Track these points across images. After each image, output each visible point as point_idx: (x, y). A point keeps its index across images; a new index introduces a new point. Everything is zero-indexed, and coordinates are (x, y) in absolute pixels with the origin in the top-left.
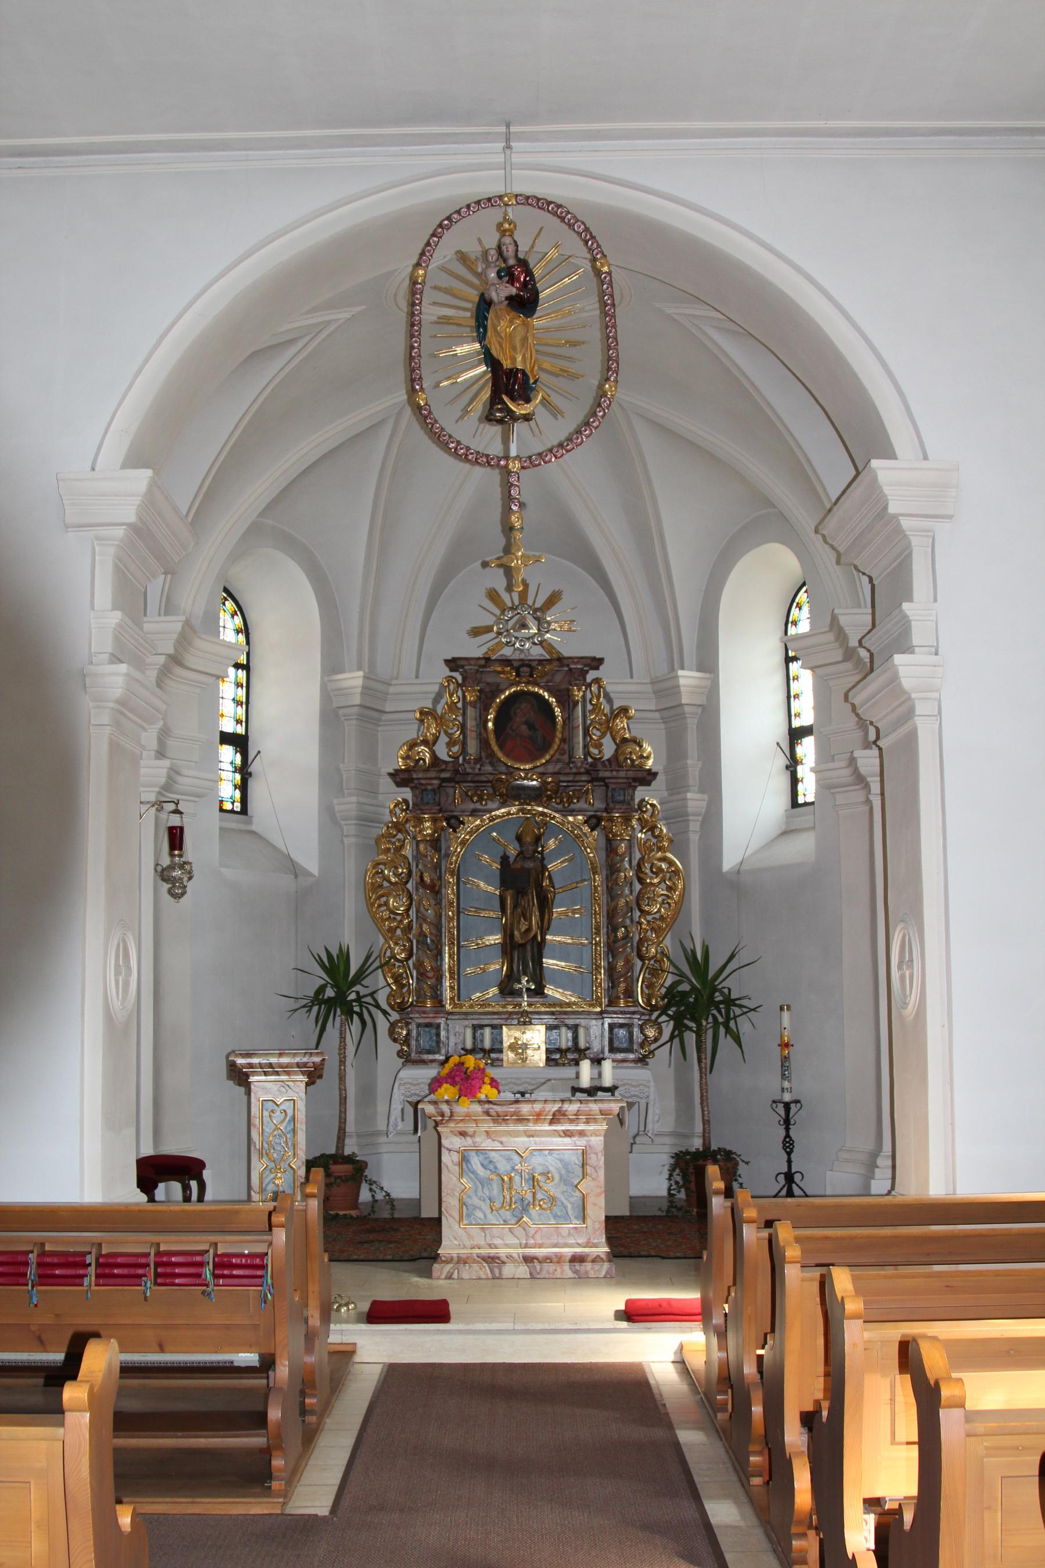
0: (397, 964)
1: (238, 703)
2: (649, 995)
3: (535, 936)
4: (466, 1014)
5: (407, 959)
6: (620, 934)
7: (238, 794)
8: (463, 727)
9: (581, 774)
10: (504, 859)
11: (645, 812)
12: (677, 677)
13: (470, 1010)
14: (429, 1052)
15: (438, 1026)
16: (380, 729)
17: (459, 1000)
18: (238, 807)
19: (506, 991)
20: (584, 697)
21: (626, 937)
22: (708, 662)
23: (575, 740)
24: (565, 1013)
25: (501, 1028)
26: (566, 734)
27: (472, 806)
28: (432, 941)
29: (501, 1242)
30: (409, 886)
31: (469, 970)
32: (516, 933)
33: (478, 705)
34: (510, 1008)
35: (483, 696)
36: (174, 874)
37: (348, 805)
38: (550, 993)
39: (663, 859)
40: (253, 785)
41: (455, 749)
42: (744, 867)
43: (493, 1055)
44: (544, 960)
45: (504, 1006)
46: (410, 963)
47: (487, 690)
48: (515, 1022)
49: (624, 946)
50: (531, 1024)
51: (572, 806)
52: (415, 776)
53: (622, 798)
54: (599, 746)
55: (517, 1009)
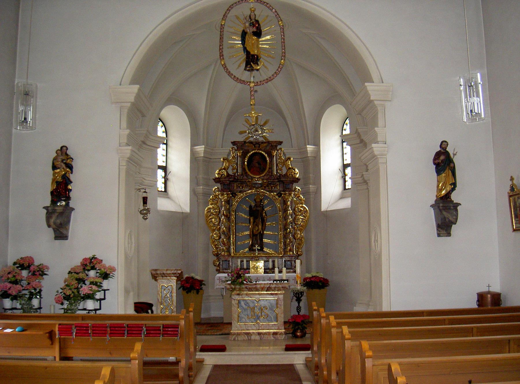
3: (260, 232)
10: (250, 207)
14: (226, 269)
15: (229, 261)
18: (163, 190)
22: (317, 143)
24: (270, 257)
30: (219, 215)
34: (252, 255)
40: (169, 184)
54: (281, 170)
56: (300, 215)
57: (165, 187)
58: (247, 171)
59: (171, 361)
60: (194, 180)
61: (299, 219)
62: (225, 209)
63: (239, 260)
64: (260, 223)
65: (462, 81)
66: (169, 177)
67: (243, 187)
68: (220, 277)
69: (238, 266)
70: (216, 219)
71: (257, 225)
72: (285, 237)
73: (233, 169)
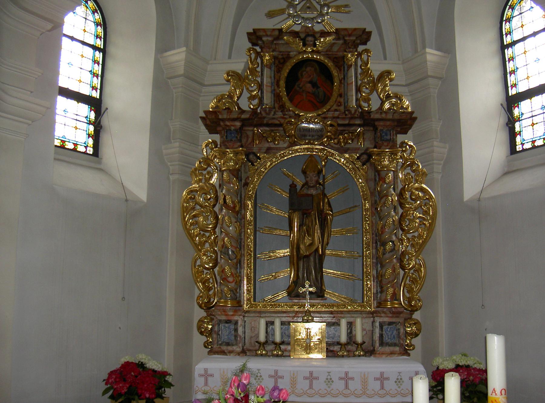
0: (205, 271)
1: (95, 75)
2: (409, 298)
3: (317, 250)
4: (260, 312)
6: (388, 247)
7: (91, 142)
8: (260, 87)
9: (356, 118)
10: (293, 186)
12: (425, 53)
13: (263, 309)
14: (228, 344)
15: (236, 323)
16: (201, 98)
17: (255, 300)
18: (90, 151)
19: (293, 294)
20: (356, 62)
21: (393, 250)
22: (446, 44)
23: (349, 94)
24: (342, 312)
26: (342, 91)
27: (267, 145)
28: (233, 252)
29: (264, 34)
30: (217, 209)
31: (263, 277)
32: (302, 246)
33: (273, 68)
34: (296, 308)
35: (277, 62)
37: (174, 148)
38: (328, 296)
39: (422, 190)
40: (105, 138)
41: (256, 102)
42: (485, 195)
43: (283, 347)
45: (291, 307)
46: (216, 270)
47: (280, 57)
49: (391, 258)
51: (347, 146)
52: (220, 117)
53: (388, 137)
54: (367, 100)
55: (302, 309)
56: (416, 209)
57: (96, 146)
58: (285, 99)
60: (159, 131)
61: (412, 221)
62: (228, 190)
63: (263, 322)
64: (317, 227)
65: (421, 167)
66: (105, 121)
67: (274, 140)
68: (206, 370)
69: (258, 336)
70: (206, 218)
72: (379, 262)
73: (252, 98)
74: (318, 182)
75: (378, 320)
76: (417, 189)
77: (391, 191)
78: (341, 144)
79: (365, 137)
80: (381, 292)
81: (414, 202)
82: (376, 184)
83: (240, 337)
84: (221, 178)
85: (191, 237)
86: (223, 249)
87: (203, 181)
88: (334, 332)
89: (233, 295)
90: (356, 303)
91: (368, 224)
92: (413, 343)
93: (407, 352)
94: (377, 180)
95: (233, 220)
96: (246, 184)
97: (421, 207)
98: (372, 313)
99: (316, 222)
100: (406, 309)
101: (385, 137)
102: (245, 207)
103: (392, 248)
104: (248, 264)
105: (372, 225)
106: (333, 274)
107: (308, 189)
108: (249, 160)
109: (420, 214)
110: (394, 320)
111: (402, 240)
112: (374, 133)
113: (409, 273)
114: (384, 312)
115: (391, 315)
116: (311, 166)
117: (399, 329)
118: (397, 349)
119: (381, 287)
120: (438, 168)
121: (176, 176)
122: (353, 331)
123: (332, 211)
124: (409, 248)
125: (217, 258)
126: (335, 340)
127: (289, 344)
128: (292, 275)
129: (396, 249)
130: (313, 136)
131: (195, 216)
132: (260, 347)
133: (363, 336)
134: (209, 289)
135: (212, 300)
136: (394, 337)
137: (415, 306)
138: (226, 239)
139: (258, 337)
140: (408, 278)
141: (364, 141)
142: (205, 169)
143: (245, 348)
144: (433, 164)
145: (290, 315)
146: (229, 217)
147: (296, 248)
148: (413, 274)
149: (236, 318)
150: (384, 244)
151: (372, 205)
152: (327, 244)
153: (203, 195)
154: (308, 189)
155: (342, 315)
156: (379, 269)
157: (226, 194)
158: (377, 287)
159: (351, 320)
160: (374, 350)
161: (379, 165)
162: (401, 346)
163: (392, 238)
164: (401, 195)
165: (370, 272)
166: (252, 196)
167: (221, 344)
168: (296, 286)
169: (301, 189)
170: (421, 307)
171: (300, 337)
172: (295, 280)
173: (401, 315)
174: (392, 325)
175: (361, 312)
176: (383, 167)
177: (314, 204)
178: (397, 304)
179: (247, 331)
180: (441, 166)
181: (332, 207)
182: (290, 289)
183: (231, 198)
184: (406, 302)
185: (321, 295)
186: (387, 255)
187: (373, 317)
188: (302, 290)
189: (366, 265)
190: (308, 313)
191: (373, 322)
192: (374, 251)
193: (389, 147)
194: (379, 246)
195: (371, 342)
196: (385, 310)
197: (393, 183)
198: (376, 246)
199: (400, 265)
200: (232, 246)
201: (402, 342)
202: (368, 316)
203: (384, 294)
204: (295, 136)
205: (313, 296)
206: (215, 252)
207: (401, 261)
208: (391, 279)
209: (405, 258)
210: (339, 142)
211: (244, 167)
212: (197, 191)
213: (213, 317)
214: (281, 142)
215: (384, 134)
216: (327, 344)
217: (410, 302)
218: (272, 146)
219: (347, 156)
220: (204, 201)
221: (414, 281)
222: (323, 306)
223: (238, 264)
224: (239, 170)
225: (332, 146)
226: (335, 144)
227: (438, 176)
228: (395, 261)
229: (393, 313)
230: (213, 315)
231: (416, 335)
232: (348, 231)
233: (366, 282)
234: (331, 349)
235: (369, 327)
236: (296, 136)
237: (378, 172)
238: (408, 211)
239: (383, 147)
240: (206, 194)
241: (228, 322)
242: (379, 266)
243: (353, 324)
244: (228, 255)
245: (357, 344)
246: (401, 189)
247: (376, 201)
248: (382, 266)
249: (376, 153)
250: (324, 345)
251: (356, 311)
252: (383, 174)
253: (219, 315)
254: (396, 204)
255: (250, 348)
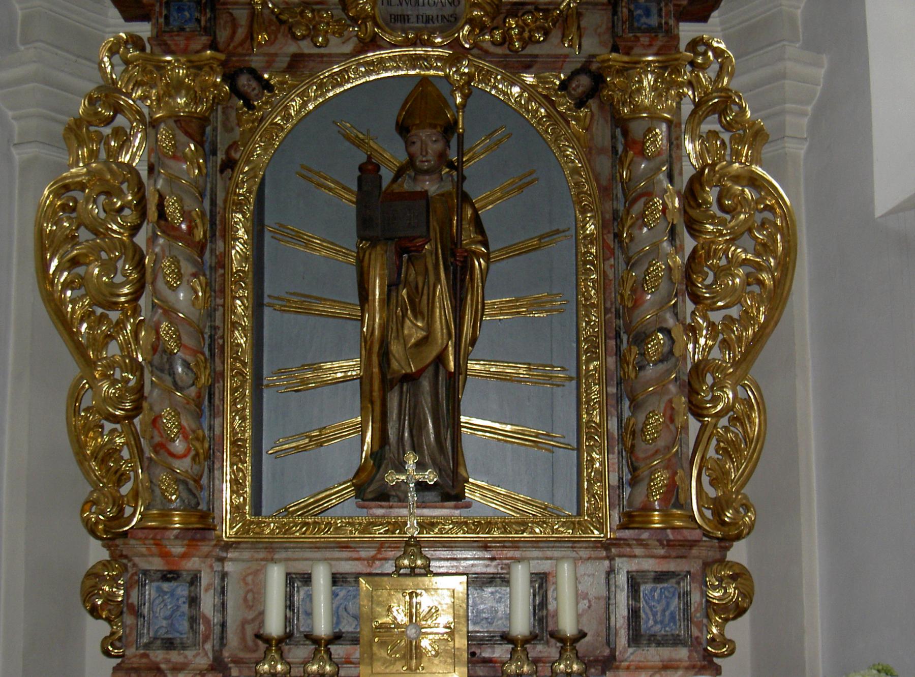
0: (109, 426)
2: (716, 501)
3: (441, 359)
5: (131, 416)
10: (369, 170)
11: (703, 67)
14: (169, 644)
15: (194, 580)
21: (667, 356)
24: (515, 545)
25: (357, 582)
30: (141, 239)
32: (395, 348)
34: (379, 533)
36: (85, 325)
38: (477, 497)
39: (754, 182)
43: (337, 650)
44: (463, 419)
45: (367, 528)
48: (614, 323)
49: (661, 381)
50: (427, 572)
53: (654, 21)
59: (243, 36)
61: (722, 273)
63: (275, 577)
64: (442, 290)
65: (749, 114)
67: (312, 34)
69: (261, 616)
70: (109, 267)
71: (419, 306)
74: (442, 157)
75: (624, 566)
76: (736, 179)
77: (660, 182)
78: (511, 43)
79: (583, 24)
80: (633, 483)
81: (728, 217)
82: (619, 160)
83: (207, 621)
84: (154, 149)
85: (65, 324)
86: (157, 357)
87: (103, 155)
88: (490, 603)
89: (185, 495)
90: (558, 516)
91: (593, 281)
92: (728, 636)
93: (711, 662)
94: (620, 149)
95: (187, 268)
96: (229, 164)
97: (750, 230)
98: (606, 545)
99: (438, 279)
100: (706, 534)
101: (644, 20)
102: (228, 234)
103: (666, 349)
104: (234, 403)
105: (603, 286)
106: (493, 430)
107: (415, 179)
108: (236, 92)
109: (745, 251)
110: (671, 566)
111: (693, 330)
112: (610, 14)
113: (715, 426)
114: (641, 543)
115: (662, 552)
116: (422, 109)
117: (687, 594)
118: (683, 653)
119: (634, 469)
120: (798, 123)
121: (31, 151)
122: (550, 599)
123: (486, 245)
124: (716, 350)
125: (142, 386)
126: (499, 626)
127: (355, 641)
128: (368, 439)
129: (677, 353)
130: (428, 19)
131: (75, 262)
132: (268, 649)
133: (579, 617)
134: (120, 478)
135: (128, 511)
136: (673, 617)
137: (734, 523)
138: (164, 325)
139: (262, 623)
140: (714, 442)
141: (580, 37)
142: (109, 121)
143: (226, 654)
144: (783, 76)
145: (363, 554)
146: (176, 261)
147: (378, 353)
148: (727, 429)
149: (193, 564)
150: (641, 339)
151: (603, 226)
152: (473, 341)
153: (103, 197)
154: (415, 179)
155: (517, 554)
156: (627, 413)
157: (163, 191)
158: (620, 468)
159: (545, 566)
160: (612, 657)
161: (624, 104)
162: (694, 643)
163: (665, 320)
164: (692, 194)
165: (599, 425)
166: (247, 198)
167: (147, 646)
168: (379, 467)
169: (395, 180)
170: (751, 527)
171: (388, 620)
172: (376, 448)
173: (695, 551)
174: (666, 580)
175: (573, 544)
176: (638, 109)
177: (434, 224)
178: (679, 517)
179: (230, 605)
180: (805, 121)
181: (488, 233)
182: (363, 476)
183: (180, 200)
184: (708, 514)
185: (453, 493)
186: (651, 371)
187: (611, 559)
188: (393, 478)
189: (588, 403)
190: (413, 546)
191: (610, 572)
192: (611, 361)
193: (654, 49)
194: (625, 345)
195: (604, 633)
196: (645, 535)
197: (665, 157)
198: (618, 347)
199: (690, 402)
200: (180, 345)
201: (695, 632)
202: (594, 554)
203: (642, 489)
204: (373, 18)
205: (431, 496)
206: (136, 368)
207: (691, 390)
208: (661, 443)
209: (704, 382)
210: (506, 39)
211: (224, 112)
212: (82, 187)
213: (125, 561)
214: (334, 40)
215: (639, 12)
216: (469, 638)
217: (718, 513)
218: (306, 51)
219: (530, 79)
220: (103, 215)
221: (729, 450)
222: (459, 524)
223: (206, 402)
224: (204, 120)
225: (486, 52)
226: (494, 43)
227: (797, 149)
228: (673, 388)
229: (670, 544)
230: (126, 557)
231: (740, 611)
232: (536, 305)
233: (589, 455)
234: (486, 654)
235: (595, 586)
236: (380, 21)
237: (621, 124)
238: (713, 242)
239: (637, 50)
240: (108, 194)
241: (170, 576)
242: (627, 403)
243: (551, 579)
244: (172, 373)
245: (562, 640)
246: (692, 180)
247: (615, 212)
248: (635, 406)
249: (618, 65)
250: (461, 642)
251: (560, 541)
252: (636, 129)
253: (143, 555)
254: (679, 220)
255: (241, 655)
